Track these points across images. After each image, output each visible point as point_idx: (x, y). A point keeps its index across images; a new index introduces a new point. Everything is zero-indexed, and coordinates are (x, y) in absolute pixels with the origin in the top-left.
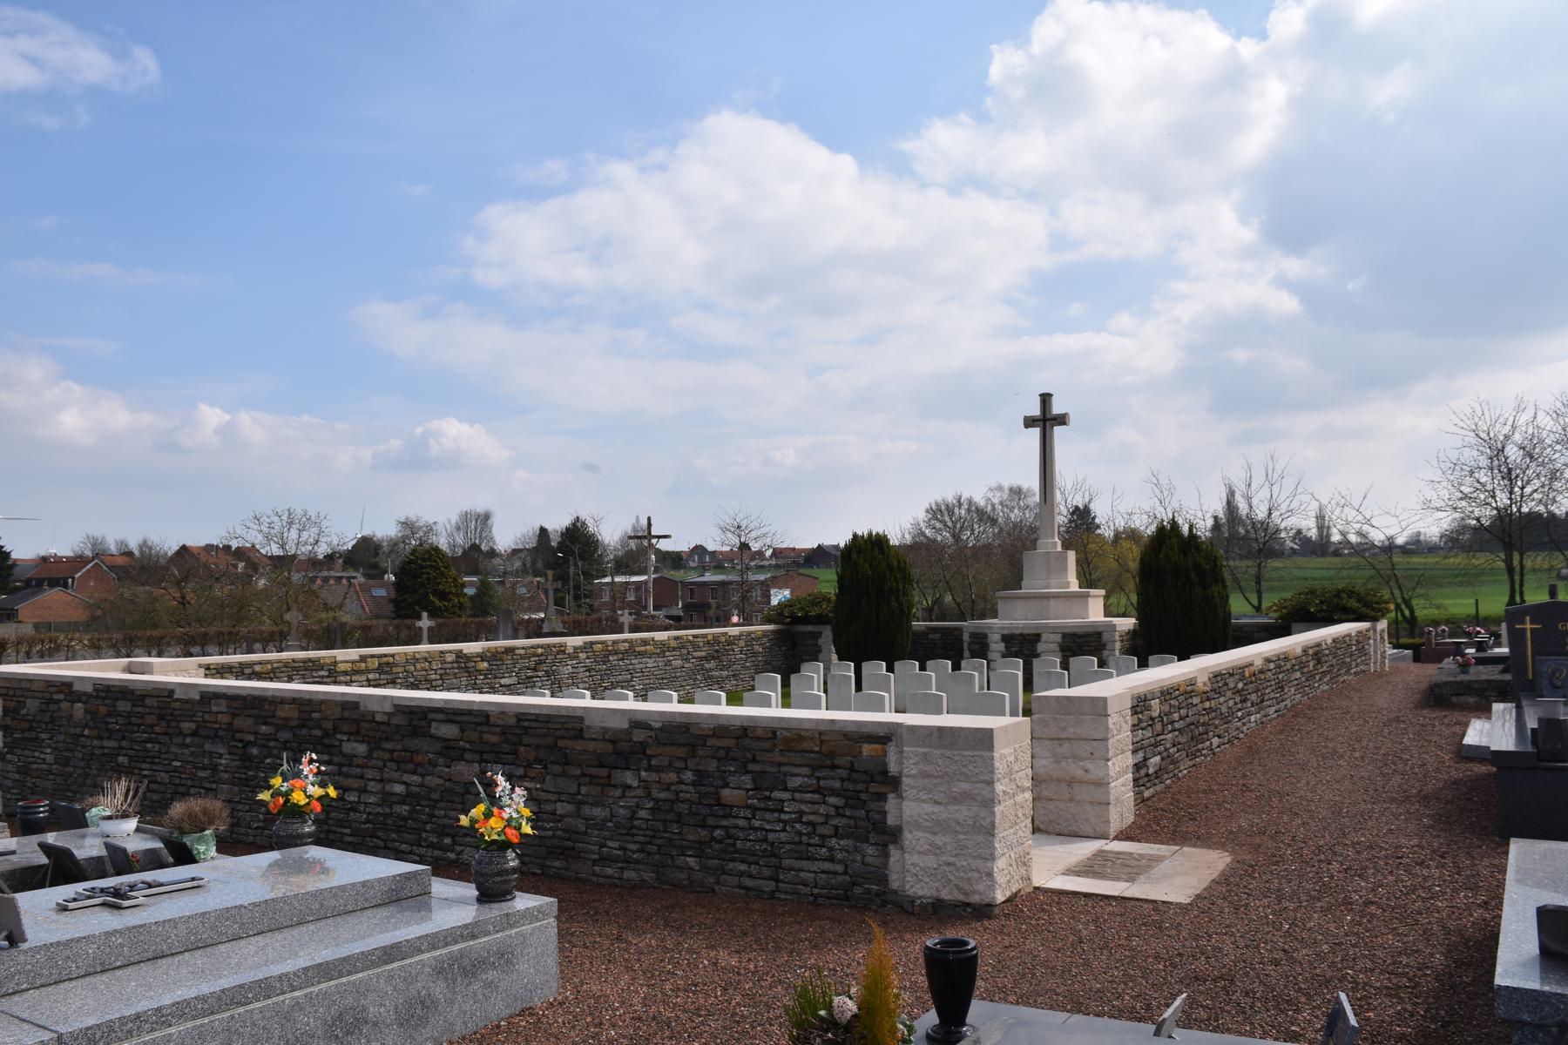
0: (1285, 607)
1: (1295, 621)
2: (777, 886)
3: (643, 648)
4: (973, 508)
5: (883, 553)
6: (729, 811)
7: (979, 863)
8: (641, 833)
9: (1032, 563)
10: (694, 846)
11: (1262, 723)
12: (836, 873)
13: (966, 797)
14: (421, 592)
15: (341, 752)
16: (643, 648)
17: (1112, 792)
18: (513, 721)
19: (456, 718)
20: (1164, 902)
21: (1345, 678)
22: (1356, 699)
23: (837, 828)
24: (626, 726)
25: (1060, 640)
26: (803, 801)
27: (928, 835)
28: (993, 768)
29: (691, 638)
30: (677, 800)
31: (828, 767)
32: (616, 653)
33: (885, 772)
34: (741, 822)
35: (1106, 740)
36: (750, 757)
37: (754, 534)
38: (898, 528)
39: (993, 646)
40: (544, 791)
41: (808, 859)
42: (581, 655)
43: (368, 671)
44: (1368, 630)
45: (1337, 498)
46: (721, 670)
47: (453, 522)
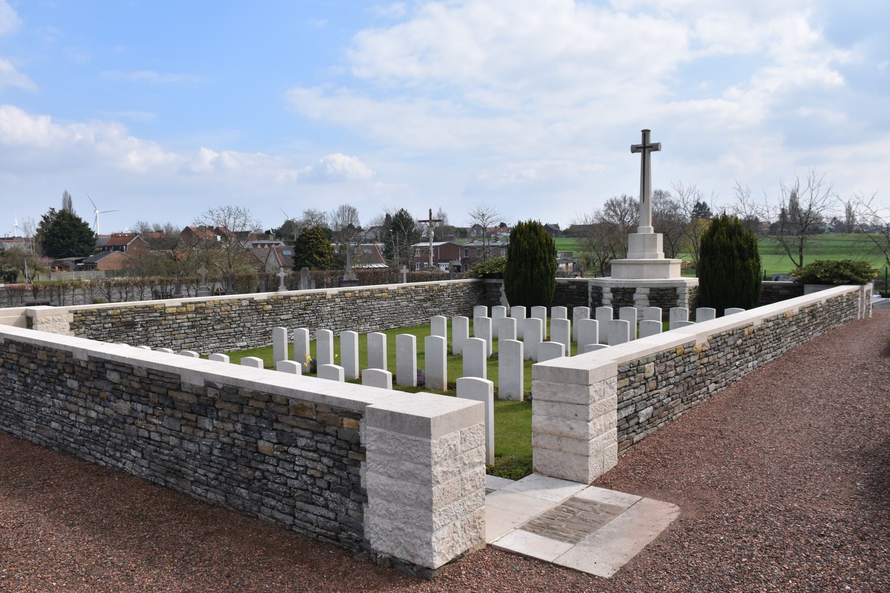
0: (800, 274)
1: (807, 283)
2: (293, 521)
3: (380, 295)
4: (633, 203)
5: (537, 234)
6: (263, 458)
7: (420, 533)
8: (215, 466)
9: (633, 240)
10: (245, 481)
11: (759, 367)
12: (329, 519)
13: (408, 475)
14: (309, 252)
15: (67, 386)
16: (380, 295)
17: (591, 447)
18: (145, 374)
19: (118, 368)
20: (588, 574)
21: (836, 325)
22: (838, 346)
23: (329, 483)
24: (203, 385)
25: (648, 293)
26: (306, 458)
27: (384, 502)
28: (430, 453)
29: (414, 288)
30: (233, 445)
31: (322, 433)
32: (362, 298)
33: (358, 444)
34: (271, 468)
35: (587, 405)
36: (275, 418)
37: (489, 220)
38: (583, 216)
39: (605, 295)
40: (163, 427)
41: (313, 504)
42: (336, 299)
43: (188, 312)
44: (857, 291)
45: (854, 199)
46: (435, 307)
47: (336, 212)
